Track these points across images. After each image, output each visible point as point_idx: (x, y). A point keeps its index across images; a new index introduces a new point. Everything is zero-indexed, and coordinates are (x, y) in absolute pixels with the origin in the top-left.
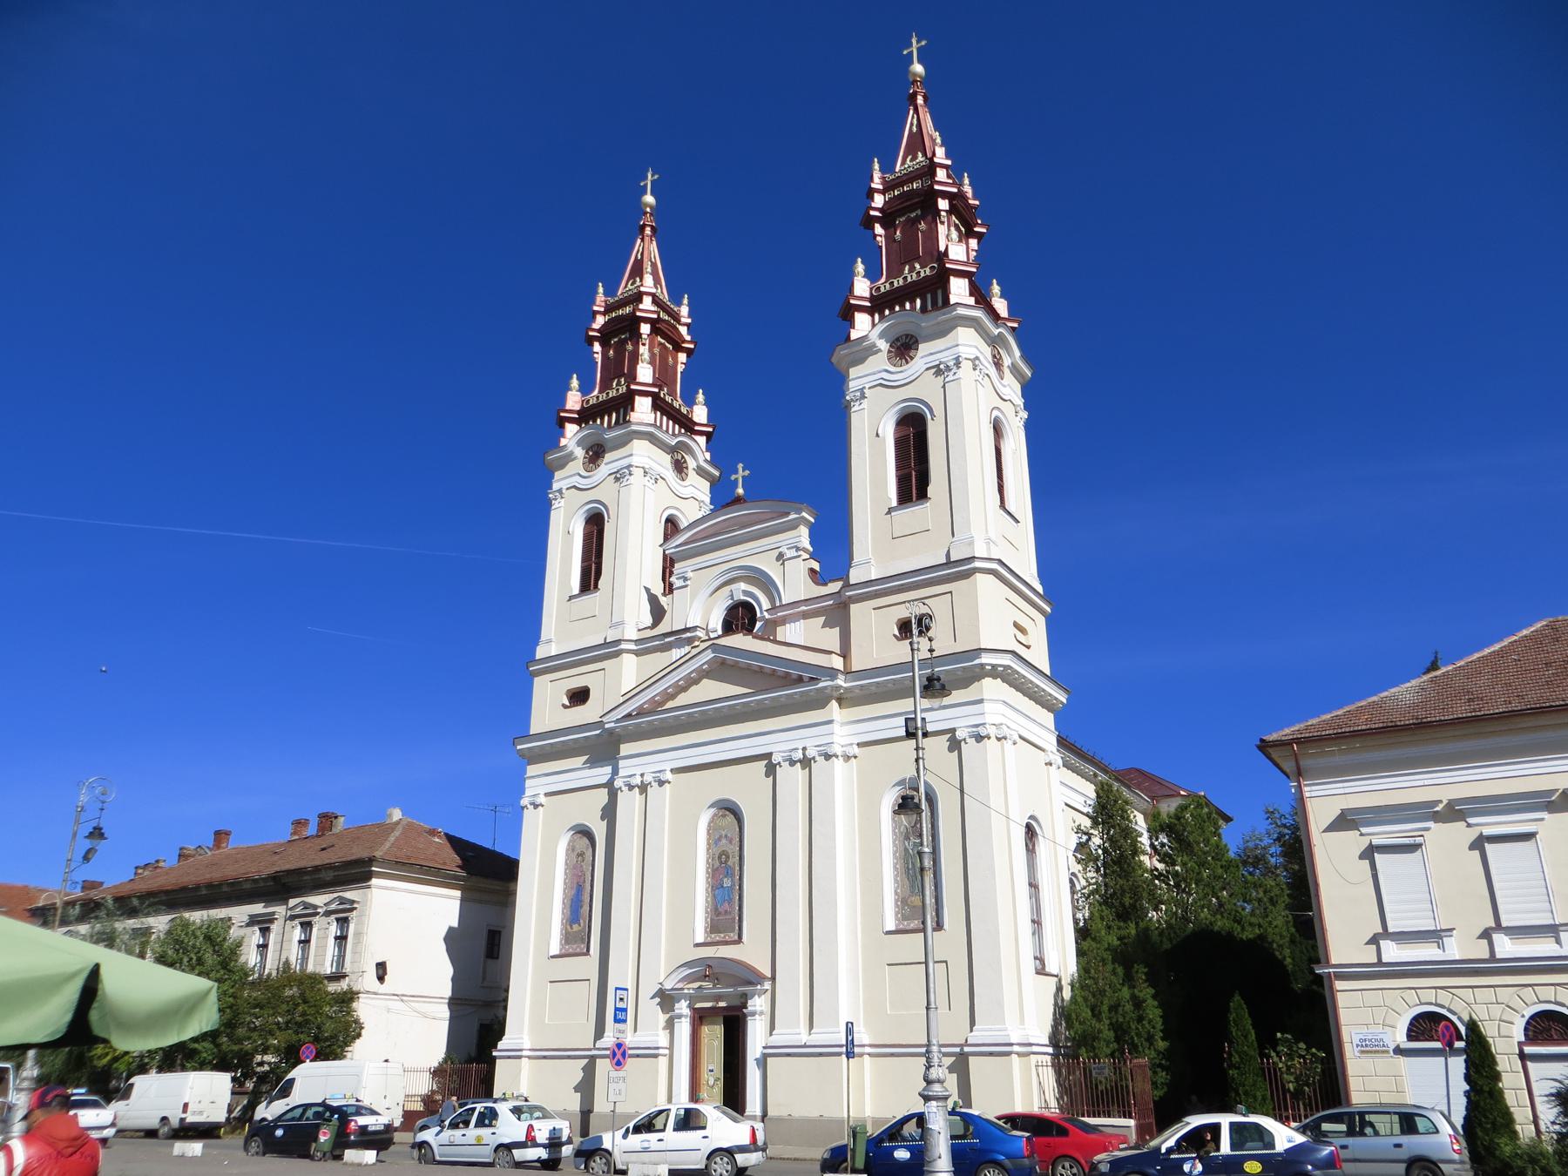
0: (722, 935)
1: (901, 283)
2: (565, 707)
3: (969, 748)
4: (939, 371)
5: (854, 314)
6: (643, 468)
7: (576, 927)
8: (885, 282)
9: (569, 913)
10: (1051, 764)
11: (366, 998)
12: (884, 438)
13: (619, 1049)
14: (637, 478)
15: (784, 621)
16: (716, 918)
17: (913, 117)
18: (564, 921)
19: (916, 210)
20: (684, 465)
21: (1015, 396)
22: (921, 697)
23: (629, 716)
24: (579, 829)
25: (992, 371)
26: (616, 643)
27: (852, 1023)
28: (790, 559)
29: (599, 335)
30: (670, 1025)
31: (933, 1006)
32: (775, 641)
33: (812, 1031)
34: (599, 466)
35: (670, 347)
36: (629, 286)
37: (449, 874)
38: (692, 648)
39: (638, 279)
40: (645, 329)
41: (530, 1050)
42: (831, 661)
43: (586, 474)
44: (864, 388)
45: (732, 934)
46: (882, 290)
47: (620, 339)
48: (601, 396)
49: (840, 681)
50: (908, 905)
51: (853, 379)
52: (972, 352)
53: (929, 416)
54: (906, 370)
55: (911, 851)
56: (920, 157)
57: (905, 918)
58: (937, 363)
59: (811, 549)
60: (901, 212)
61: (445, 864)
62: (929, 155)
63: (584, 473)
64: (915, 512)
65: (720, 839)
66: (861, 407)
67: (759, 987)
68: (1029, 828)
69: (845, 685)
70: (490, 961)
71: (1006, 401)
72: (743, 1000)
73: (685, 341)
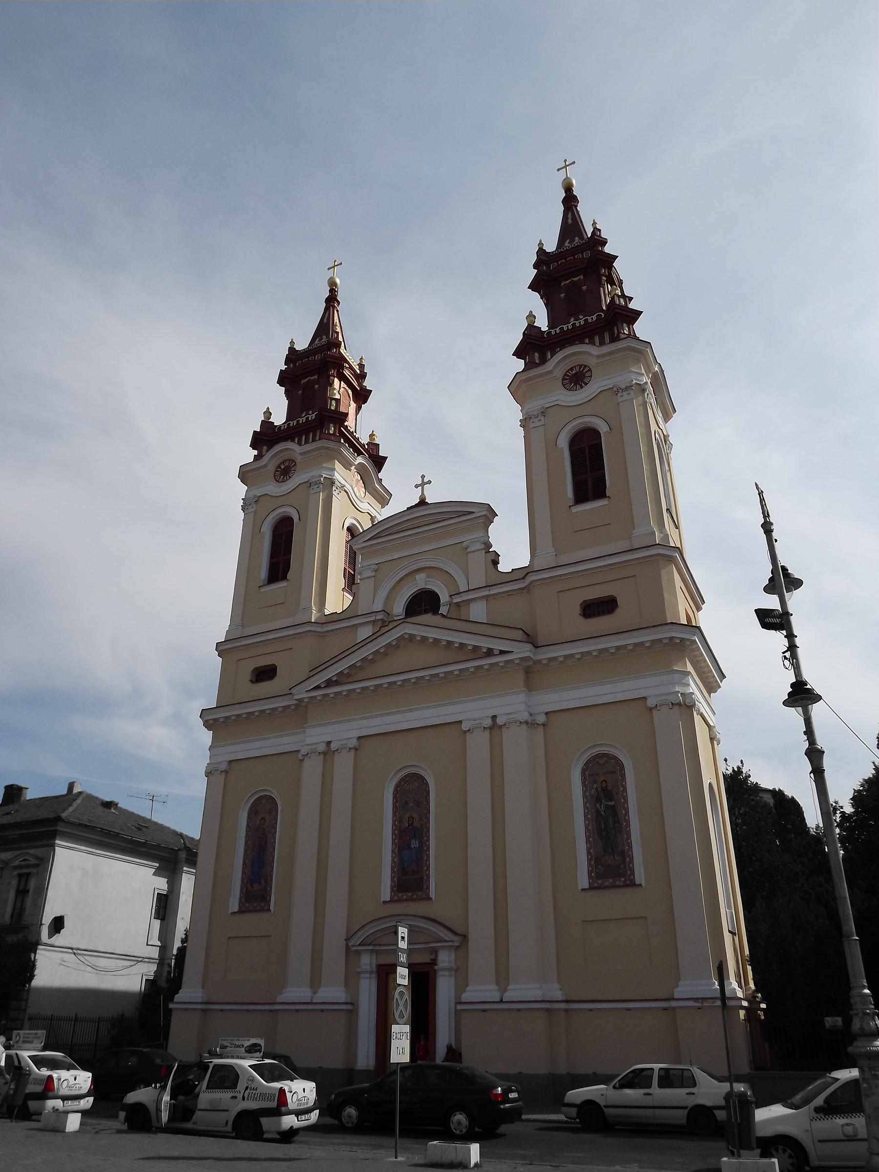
0: (410, 894)
7: (256, 887)
11: (44, 949)
19: (315, 375)
23: (317, 688)
37: (127, 839)
41: (201, 1003)
43: (345, 528)
45: (420, 893)
57: (399, 891)
61: (122, 830)
72: (433, 957)
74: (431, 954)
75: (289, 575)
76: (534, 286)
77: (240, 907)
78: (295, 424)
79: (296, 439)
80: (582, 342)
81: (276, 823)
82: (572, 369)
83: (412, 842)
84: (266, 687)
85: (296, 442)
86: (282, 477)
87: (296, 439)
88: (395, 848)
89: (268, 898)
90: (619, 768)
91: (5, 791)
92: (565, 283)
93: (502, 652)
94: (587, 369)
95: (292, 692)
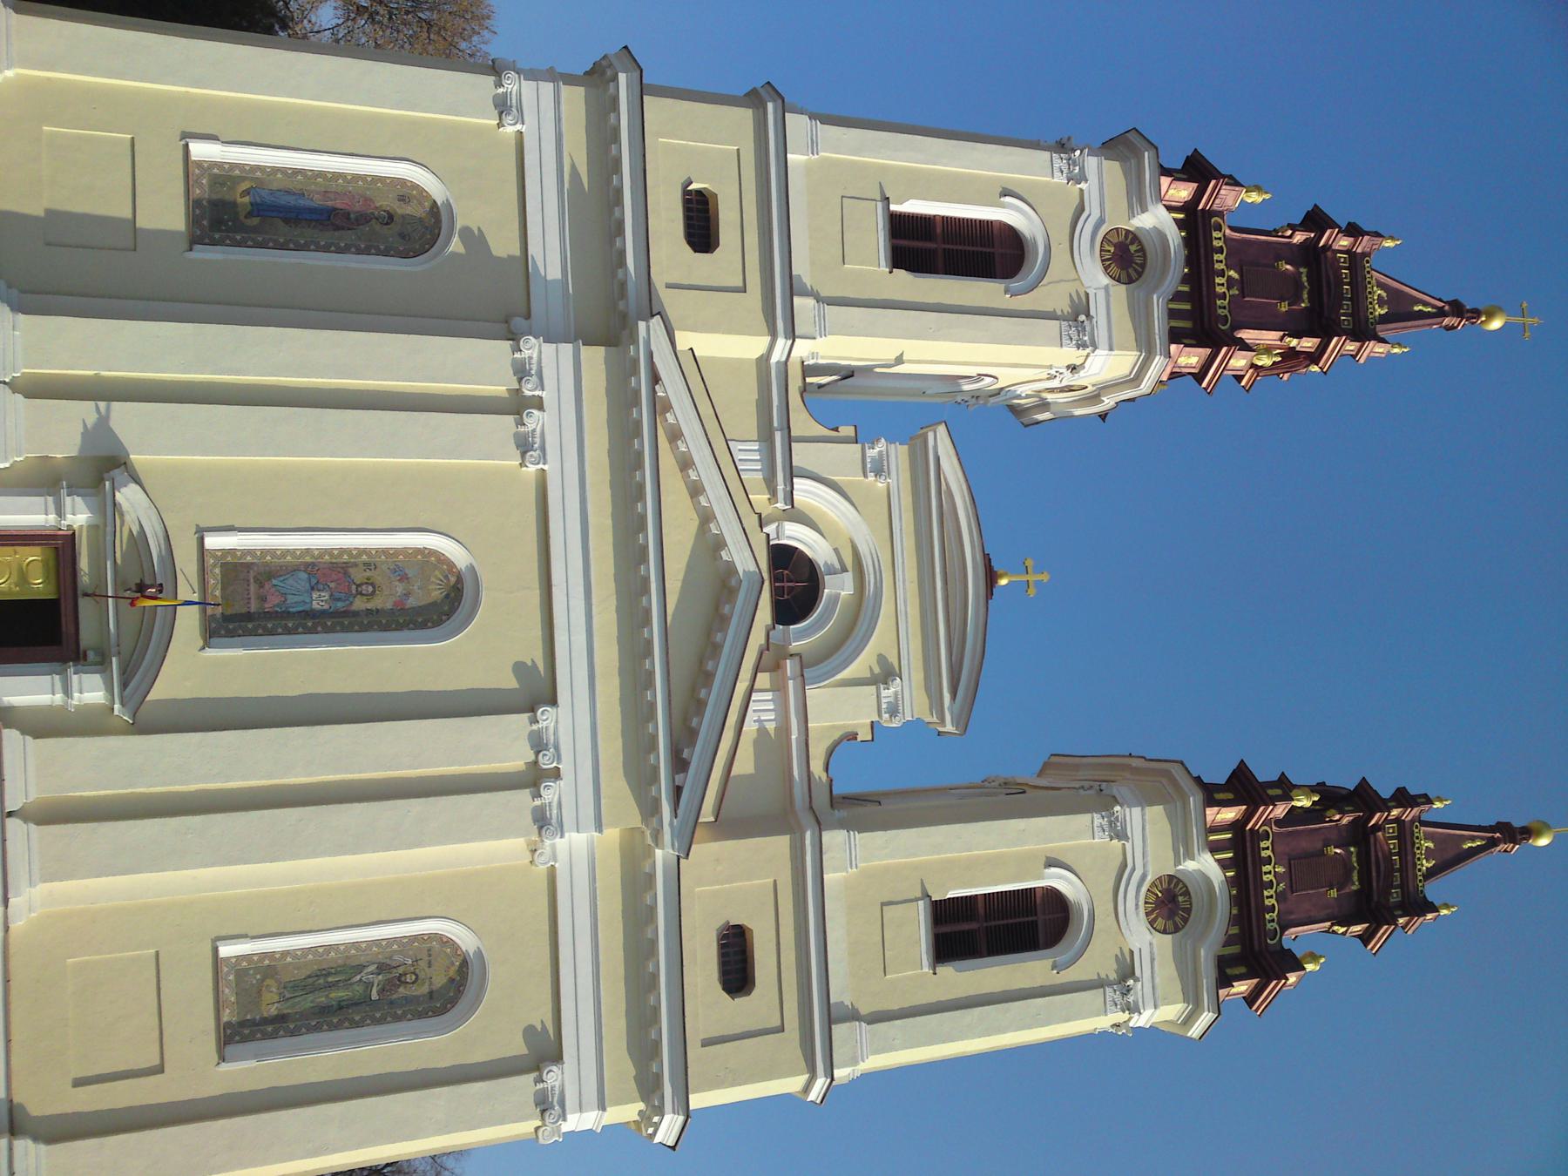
1: (1218, 266)
4: (1127, 970)
9: (275, 186)
12: (1003, 206)
16: (252, 574)
17: (1433, 306)
23: (655, 379)
24: (473, 979)
28: (878, 696)
46: (1215, 234)
47: (1303, 287)
50: (263, 980)
53: (1060, 959)
54: (1137, 914)
55: (358, 977)
56: (1381, 311)
57: (226, 567)
60: (1315, 279)
64: (877, 241)
65: (404, 578)
75: (901, 274)
76: (1364, 782)
77: (199, 164)
78: (1220, 311)
79: (1186, 289)
80: (1234, 920)
83: (323, 594)
84: (668, 220)
85: (1180, 288)
87: (1186, 289)
88: (313, 556)
90: (438, 1005)
93: (678, 791)
94: (1134, 275)
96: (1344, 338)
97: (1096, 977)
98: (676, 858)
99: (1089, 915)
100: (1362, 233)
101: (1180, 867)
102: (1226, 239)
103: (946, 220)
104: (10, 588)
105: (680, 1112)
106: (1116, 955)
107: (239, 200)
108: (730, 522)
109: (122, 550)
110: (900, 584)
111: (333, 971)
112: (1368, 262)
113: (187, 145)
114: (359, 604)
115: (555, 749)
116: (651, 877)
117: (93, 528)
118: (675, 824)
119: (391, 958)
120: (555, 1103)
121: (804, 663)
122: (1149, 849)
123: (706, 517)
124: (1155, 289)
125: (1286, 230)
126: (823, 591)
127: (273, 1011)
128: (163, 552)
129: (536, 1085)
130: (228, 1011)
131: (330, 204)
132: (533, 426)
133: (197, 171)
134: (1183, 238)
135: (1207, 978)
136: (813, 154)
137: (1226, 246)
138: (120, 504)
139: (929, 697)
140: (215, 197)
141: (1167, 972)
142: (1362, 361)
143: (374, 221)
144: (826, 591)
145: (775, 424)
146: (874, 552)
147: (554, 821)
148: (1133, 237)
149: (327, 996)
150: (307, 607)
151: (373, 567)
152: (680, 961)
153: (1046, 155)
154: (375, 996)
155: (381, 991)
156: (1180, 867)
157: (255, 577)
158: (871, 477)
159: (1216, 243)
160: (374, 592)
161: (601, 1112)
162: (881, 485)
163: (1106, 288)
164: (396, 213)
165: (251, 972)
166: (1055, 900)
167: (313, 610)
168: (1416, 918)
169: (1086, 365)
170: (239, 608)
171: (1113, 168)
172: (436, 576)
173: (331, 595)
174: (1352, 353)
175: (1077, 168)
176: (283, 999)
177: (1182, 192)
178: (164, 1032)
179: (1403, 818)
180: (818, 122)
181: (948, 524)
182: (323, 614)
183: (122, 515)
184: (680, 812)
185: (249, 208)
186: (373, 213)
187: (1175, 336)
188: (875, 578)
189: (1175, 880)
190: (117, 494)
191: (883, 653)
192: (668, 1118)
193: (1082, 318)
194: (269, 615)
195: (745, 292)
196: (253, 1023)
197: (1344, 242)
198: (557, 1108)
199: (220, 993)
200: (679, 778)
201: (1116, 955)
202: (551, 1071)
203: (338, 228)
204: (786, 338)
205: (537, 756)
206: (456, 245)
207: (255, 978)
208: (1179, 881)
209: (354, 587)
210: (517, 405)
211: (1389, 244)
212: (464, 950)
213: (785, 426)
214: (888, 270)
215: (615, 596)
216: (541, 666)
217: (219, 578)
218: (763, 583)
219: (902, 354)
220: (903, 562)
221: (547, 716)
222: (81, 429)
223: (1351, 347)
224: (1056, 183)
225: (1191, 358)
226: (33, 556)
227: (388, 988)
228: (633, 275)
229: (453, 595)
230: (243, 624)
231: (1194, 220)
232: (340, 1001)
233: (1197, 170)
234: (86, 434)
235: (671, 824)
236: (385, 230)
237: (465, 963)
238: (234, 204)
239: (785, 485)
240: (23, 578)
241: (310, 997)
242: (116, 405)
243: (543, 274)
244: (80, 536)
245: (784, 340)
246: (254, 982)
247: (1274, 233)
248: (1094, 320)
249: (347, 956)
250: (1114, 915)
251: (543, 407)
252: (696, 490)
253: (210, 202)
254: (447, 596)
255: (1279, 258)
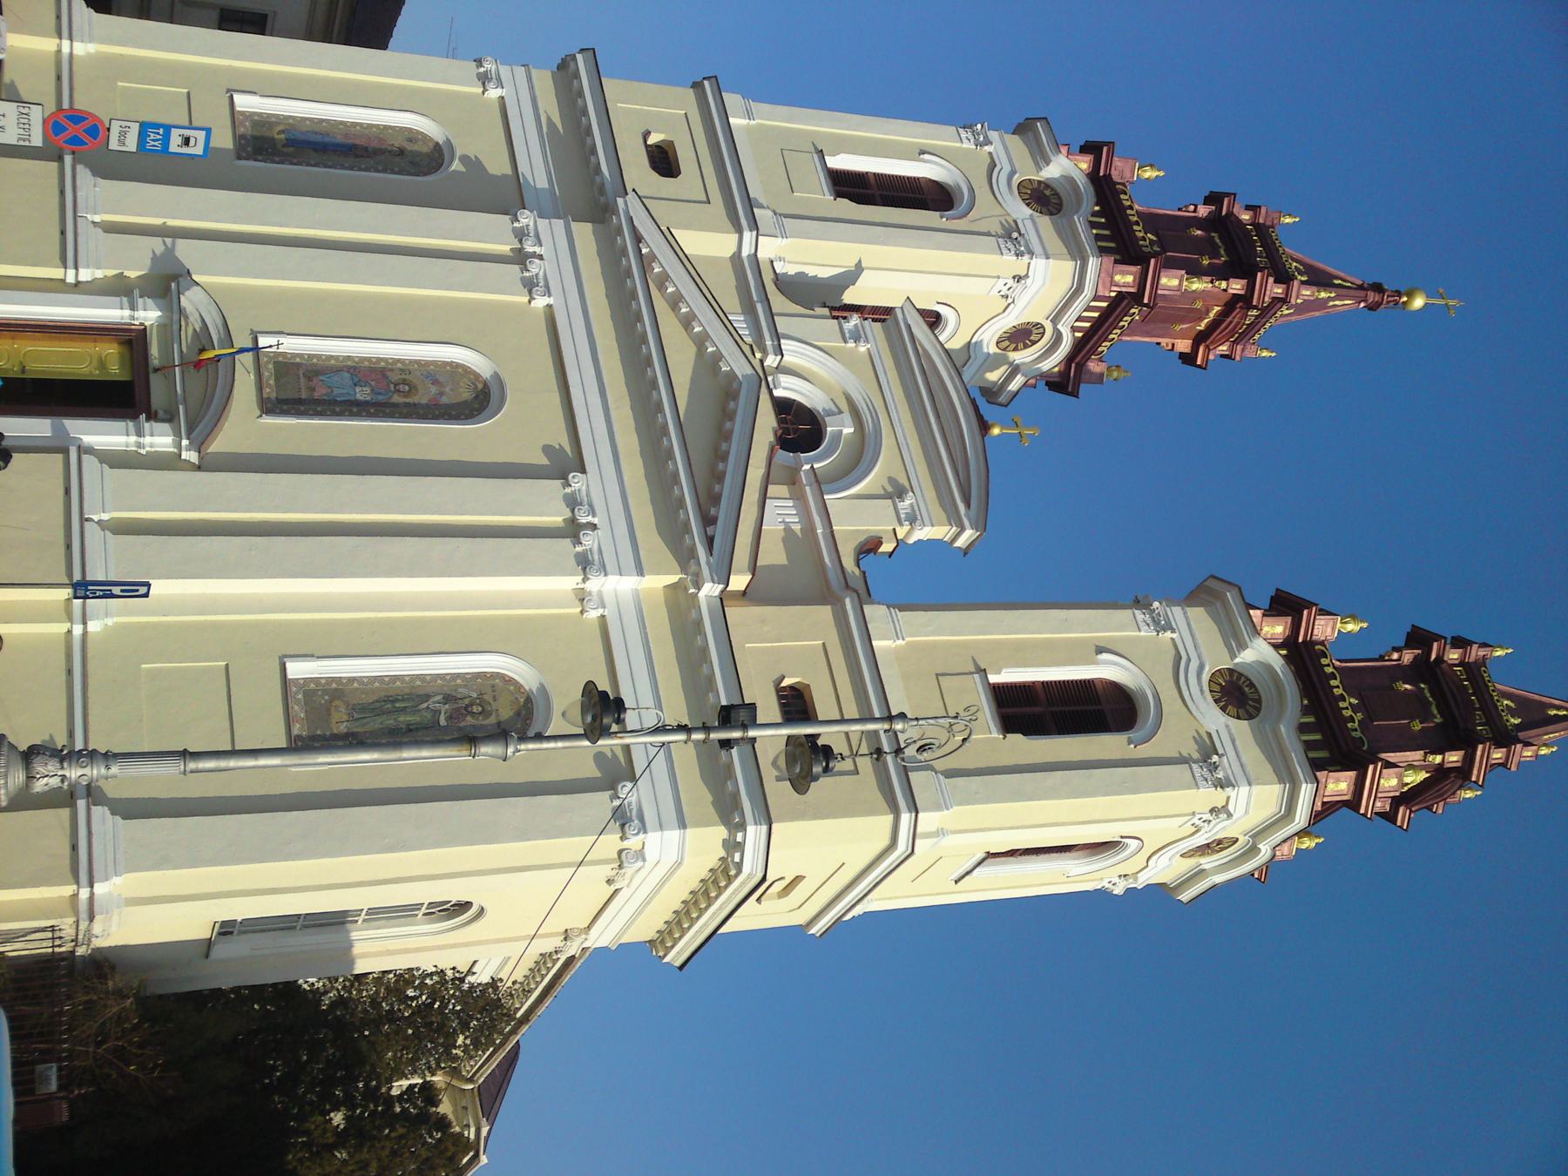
0: (272, 382)
2: (646, 135)
3: (601, 803)
4: (1207, 751)
5: (1287, 615)
6: (1027, 276)
8: (1334, 667)
9: (305, 129)
10: (565, 939)
12: (1096, 663)
13: (89, 132)
14: (1009, 263)
15: (798, 497)
18: (291, 121)
20: (1021, 345)
21: (1151, 873)
22: (789, 737)
23: (638, 239)
25: (1200, 840)
26: (752, 224)
27: (146, 595)
29: (1224, 213)
30: (118, 288)
31: (192, 765)
32: (767, 481)
33: (108, 533)
34: (1028, 205)
35: (1202, 326)
36: (1295, 264)
38: (751, 346)
39: (1304, 278)
40: (1237, 286)
42: (740, 572)
44: (1173, 631)
47: (1430, 703)
48: (1133, 212)
49: (710, 590)
50: (331, 701)
51: (1185, 613)
52: (1236, 807)
54: (1205, 698)
55: (425, 705)
58: (1220, 751)
59: (911, 541)
62: (1521, 735)
63: (1016, 179)
65: (435, 382)
66: (1142, 625)
67: (185, 442)
68: (464, 906)
69: (702, 594)
70: (215, 15)
71: (1147, 862)
72: (161, 414)
73: (1208, 349)
74: (165, 411)
77: (242, 113)
78: (1354, 734)
79: (1311, 719)
81: (393, 172)
82: (1252, 685)
83: (364, 389)
85: (1303, 720)
86: (1029, 192)
87: (1311, 719)
89: (260, 158)
91: (497, 176)
92: (1426, 691)
95: (629, 196)
96: (1488, 744)
97: (1178, 755)
98: (719, 600)
99: (1154, 697)
100: (1470, 643)
101: (1237, 660)
102: (1139, 214)
103: (1047, 685)
104: (91, 372)
105: (763, 822)
106: (1194, 737)
107: (276, 136)
108: (730, 355)
109: (187, 342)
110: (885, 387)
111: (400, 698)
112: (1273, 232)
113: (232, 96)
114: (397, 399)
115: (589, 505)
116: (699, 623)
117: (163, 327)
118: (712, 561)
119: (456, 691)
120: (634, 818)
121: (818, 481)
122: (1200, 642)
123: (701, 341)
124: (1279, 719)
125: (1392, 654)
126: (826, 430)
127: (343, 728)
128: (222, 336)
129: (612, 802)
130: (298, 725)
131: (350, 141)
132: (537, 270)
133: (241, 117)
134: (1284, 657)
135: (1295, 751)
136: (750, 119)
137: (1346, 692)
138: (185, 308)
139: (945, 510)
140: (256, 133)
141: (1252, 754)
142: (1514, 768)
143: (387, 154)
144: (829, 429)
145: (755, 298)
146: (866, 397)
147: (597, 562)
148: (1045, 185)
149: (395, 720)
150: (352, 398)
151: (408, 372)
152: (737, 682)
153: (1128, 612)
154: (443, 722)
155: (449, 718)
156: (1237, 660)
157: (303, 374)
158: (851, 344)
159: (1329, 670)
160: (410, 391)
161: (682, 831)
162: (863, 349)
163: (1031, 215)
164: (406, 149)
165: (320, 693)
166: (1116, 690)
167: (357, 400)
168: (1513, 747)
169: (1029, 274)
170: (289, 394)
171: (1198, 614)
172: (464, 382)
173: (372, 390)
174: (1500, 761)
175: (982, 136)
176: (352, 719)
177: (1278, 628)
178: (235, 733)
179: (1467, 660)
180: (897, 610)
181: (933, 381)
182: (366, 403)
183: (187, 318)
184: (715, 552)
185: (285, 142)
186: (386, 149)
187: (1316, 766)
188: (872, 416)
189: (1236, 675)
190: (182, 298)
191: (892, 475)
192: (751, 829)
193: (1015, 235)
194: (318, 402)
195: (858, 774)
196: (323, 738)
197: (1453, 655)
198: (636, 822)
199: (290, 709)
200: (710, 530)
201: (1194, 737)
202: (624, 786)
203: (357, 156)
204: (751, 231)
205: (573, 511)
206: (456, 165)
207: (323, 699)
208: (1240, 675)
209: (392, 386)
210: (573, 530)
211: (1499, 653)
212: (527, 688)
213: (764, 298)
214: (832, 198)
215: (628, 398)
216: (568, 449)
217: (273, 371)
218: (761, 381)
219: (860, 261)
220: (896, 407)
221: (577, 482)
222: (151, 255)
223: (1498, 755)
224: (1143, 636)
225: (1339, 785)
226: (110, 351)
227: (455, 716)
228: (608, 177)
229: (481, 397)
230: (296, 406)
231: (1300, 653)
232: (409, 725)
233: (1285, 605)
234: (155, 258)
235: (708, 563)
236: (397, 159)
237: (529, 700)
238: (273, 139)
239: (773, 341)
240: (102, 364)
241: (379, 719)
242: (180, 242)
243: (533, 184)
244: (151, 334)
245: (749, 233)
246: (323, 702)
247: (1381, 658)
248: (1026, 235)
249: (413, 687)
250: (1180, 700)
251: (585, 470)
252: (687, 322)
253: (251, 136)
254: (476, 397)
255: (1396, 680)
